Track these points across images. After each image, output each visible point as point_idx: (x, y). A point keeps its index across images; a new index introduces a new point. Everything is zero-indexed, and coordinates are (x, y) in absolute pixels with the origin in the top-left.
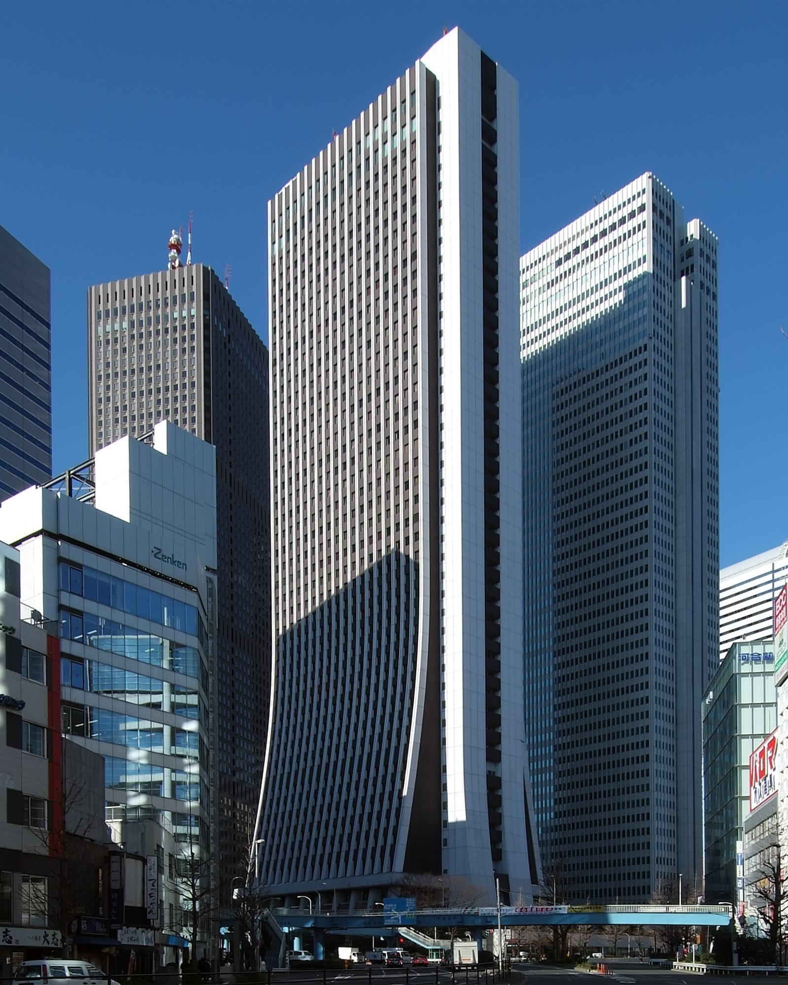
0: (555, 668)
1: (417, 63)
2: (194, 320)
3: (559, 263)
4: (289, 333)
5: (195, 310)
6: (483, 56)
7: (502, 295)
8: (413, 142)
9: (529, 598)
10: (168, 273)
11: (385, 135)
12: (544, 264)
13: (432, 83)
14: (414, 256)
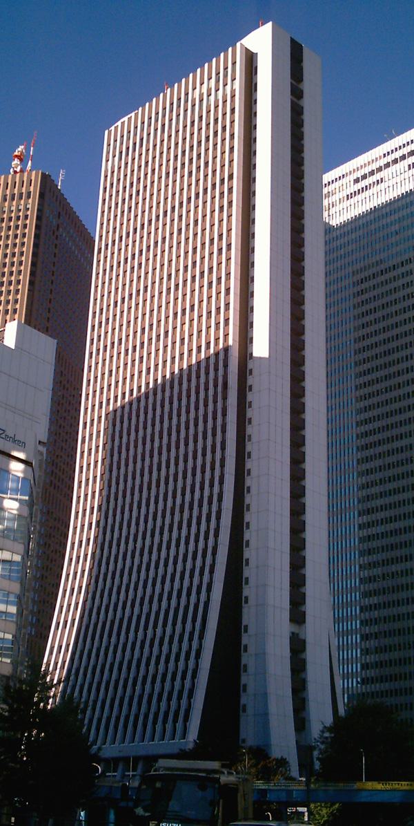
0: (359, 502)
1: (238, 45)
2: (29, 213)
3: (357, 181)
4: (115, 229)
5: (33, 204)
6: (292, 41)
7: (307, 194)
8: (233, 96)
9: (335, 512)
10: (10, 176)
11: (209, 90)
12: (344, 181)
13: (251, 60)
14: (231, 177)
